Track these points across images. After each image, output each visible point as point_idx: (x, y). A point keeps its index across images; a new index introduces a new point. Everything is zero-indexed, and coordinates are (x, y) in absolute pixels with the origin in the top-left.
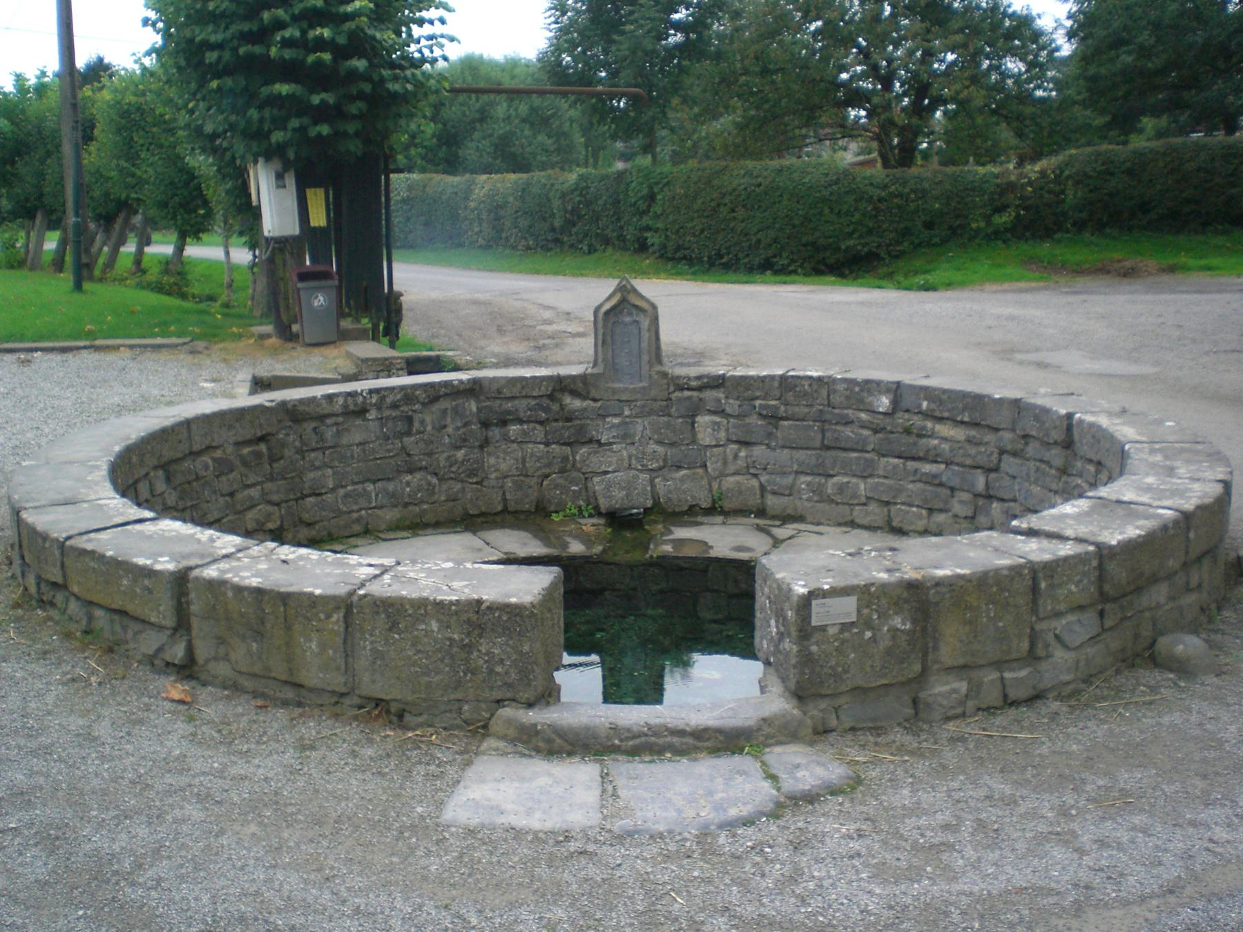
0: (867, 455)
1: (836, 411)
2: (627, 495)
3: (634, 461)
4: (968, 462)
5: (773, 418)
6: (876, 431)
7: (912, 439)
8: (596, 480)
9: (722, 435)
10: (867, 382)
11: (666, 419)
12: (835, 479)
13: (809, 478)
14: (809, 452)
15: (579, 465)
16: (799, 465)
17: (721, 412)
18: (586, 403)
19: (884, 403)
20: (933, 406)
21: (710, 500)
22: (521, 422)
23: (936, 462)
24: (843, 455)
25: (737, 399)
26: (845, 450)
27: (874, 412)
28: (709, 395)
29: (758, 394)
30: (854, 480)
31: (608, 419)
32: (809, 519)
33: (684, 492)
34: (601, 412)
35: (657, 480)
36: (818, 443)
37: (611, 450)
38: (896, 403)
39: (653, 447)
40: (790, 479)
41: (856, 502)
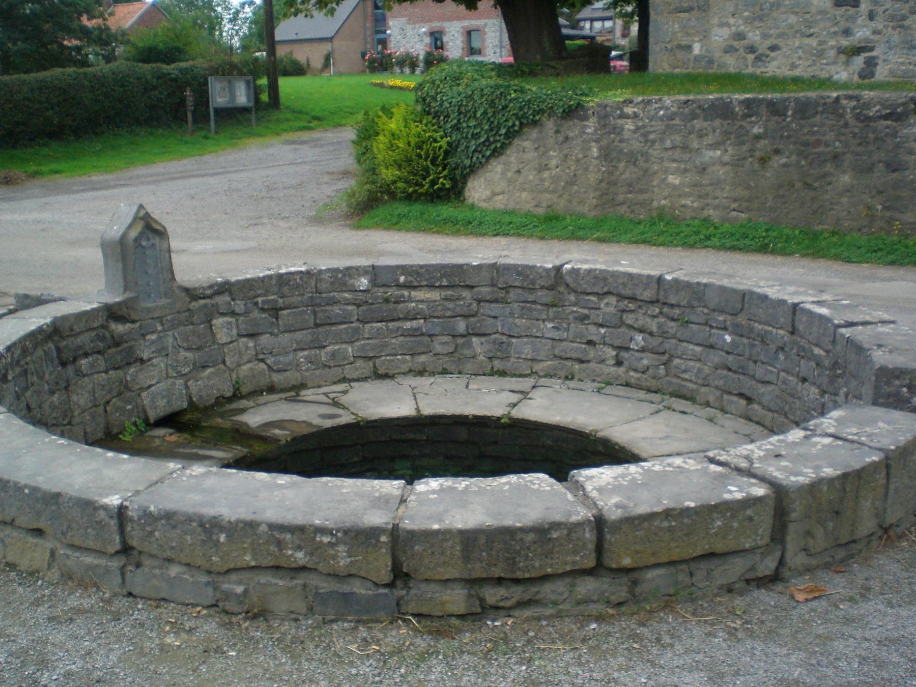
0: (353, 325)
1: (324, 295)
2: (168, 402)
3: (170, 371)
4: (449, 313)
5: (275, 311)
6: (358, 306)
7: (391, 306)
8: (144, 394)
9: (235, 332)
10: (348, 269)
11: (191, 327)
12: (329, 349)
13: (306, 353)
14: (305, 332)
15: (130, 385)
16: (297, 344)
17: (233, 314)
18: (128, 326)
19: (364, 282)
20: (410, 278)
21: (232, 390)
22: (86, 355)
23: (416, 319)
24: (334, 328)
25: (242, 300)
26: (332, 324)
27: (356, 291)
28: (224, 299)
29: (259, 292)
30: (344, 346)
31: (148, 337)
32: (310, 385)
33: (211, 388)
34: (142, 332)
35: (190, 383)
36: (312, 324)
37: (153, 365)
38: (374, 283)
39: (183, 354)
40: (291, 356)
41: (345, 362)
